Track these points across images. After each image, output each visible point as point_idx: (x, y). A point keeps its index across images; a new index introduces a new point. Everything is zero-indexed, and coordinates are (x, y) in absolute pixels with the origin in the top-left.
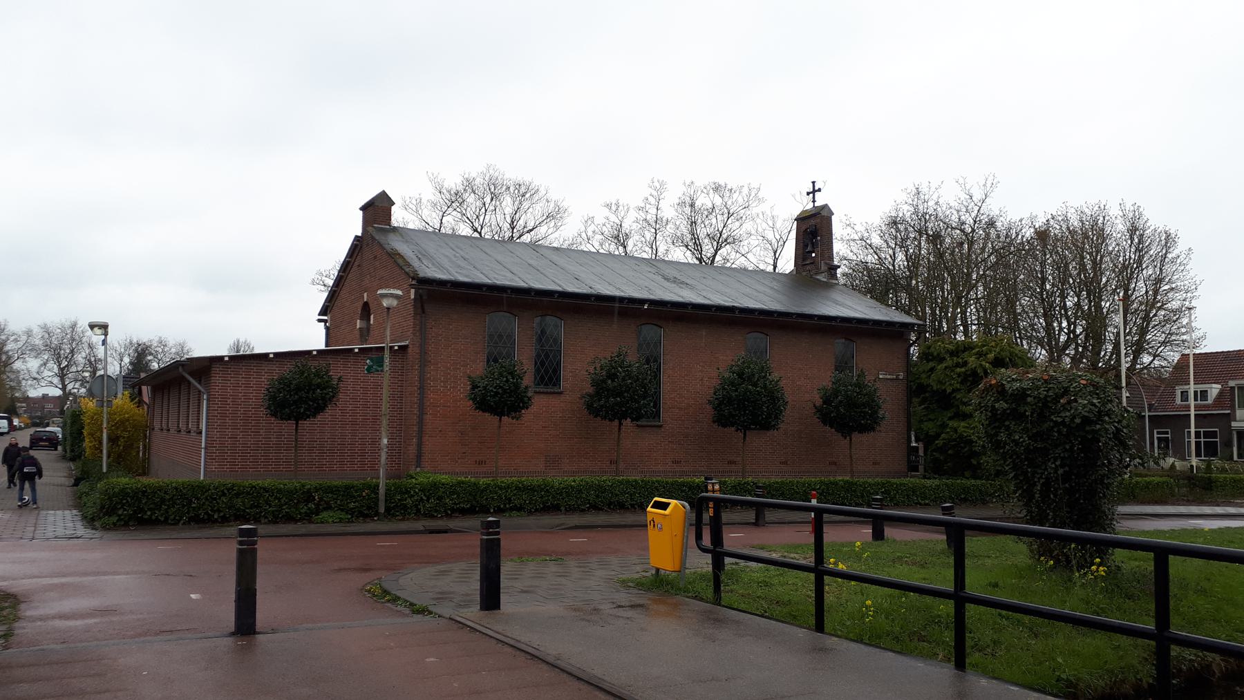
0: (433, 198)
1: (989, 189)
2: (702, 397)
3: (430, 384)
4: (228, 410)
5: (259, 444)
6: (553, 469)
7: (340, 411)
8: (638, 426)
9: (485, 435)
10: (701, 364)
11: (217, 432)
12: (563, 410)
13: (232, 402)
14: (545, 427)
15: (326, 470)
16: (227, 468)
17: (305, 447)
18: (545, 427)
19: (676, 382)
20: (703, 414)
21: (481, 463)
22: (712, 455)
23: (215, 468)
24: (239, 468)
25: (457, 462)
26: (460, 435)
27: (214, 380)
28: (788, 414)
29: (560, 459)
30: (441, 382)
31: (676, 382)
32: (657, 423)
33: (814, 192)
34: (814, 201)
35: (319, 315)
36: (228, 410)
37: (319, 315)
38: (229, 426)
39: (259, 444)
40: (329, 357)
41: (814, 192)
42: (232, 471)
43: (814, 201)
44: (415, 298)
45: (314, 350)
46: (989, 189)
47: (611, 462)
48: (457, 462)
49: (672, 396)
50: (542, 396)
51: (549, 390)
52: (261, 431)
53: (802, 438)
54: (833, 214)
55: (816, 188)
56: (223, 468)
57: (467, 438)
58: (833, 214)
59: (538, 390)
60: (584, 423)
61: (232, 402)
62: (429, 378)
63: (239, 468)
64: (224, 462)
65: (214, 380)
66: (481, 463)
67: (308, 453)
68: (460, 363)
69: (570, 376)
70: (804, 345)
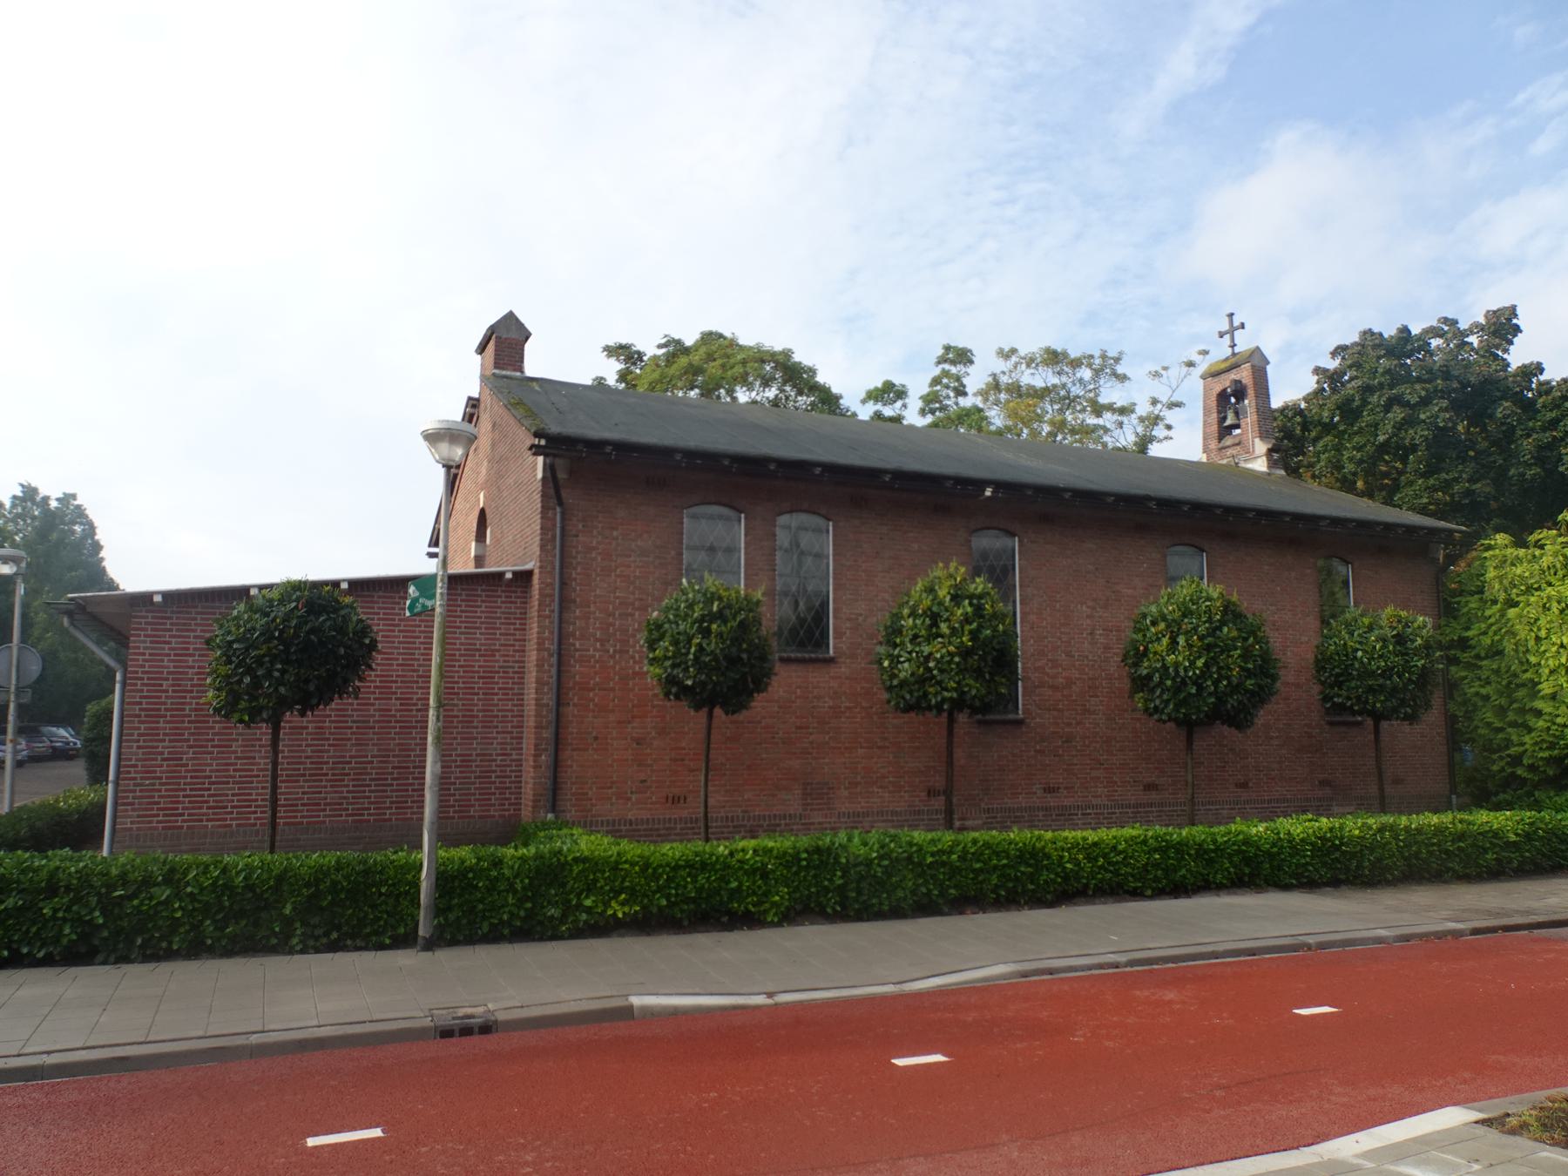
0: (966, 716)
1: (1503, 326)
2: (1093, 666)
3: (574, 645)
4: (165, 704)
5: (228, 770)
6: (819, 810)
7: (398, 702)
8: (979, 722)
9: (683, 745)
10: (1090, 603)
11: (139, 747)
12: (835, 693)
13: (173, 685)
14: (800, 728)
15: (231, 825)
16: (158, 822)
17: (327, 775)
18: (800, 728)
19: (1046, 637)
20: (1098, 697)
21: (675, 800)
22: (1115, 774)
23: (132, 823)
24: (184, 821)
25: (629, 799)
26: (635, 745)
27: (135, 642)
28: (1287, 676)
29: (829, 788)
30: (597, 640)
31: (1046, 637)
32: (1011, 716)
33: (1232, 331)
34: (1233, 346)
35: (430, 546)
36: (165, 704)
37: (430, 546)
38: (165, 734)
39: (228, 770)
40: (376, 594)
41: (1232, 331)
42: (170, 828)
43: (1233, 346)
44: (544, 478)
45: (344, 580)
46: (1503, 326)
47: (929, 792)
48: (629, 799)
49: (1038, 664)
50: (793, 667)
51: (806, 656)
52: (234, 744)
53: (1272, 738)
54: (1268, 363)
55: (1227, 337)
56: (150, 822)
57: (649, 751)
58: (1268, 363)
59: (785, 655)
60: (875, 718)
61: (173, 685)
62: (573, 634)
63: (184, 821)
64: (152, 809)
65: (135, 642)
66: (675, 800)
67: (331, 786)
68: (633, 604)
69: (847, 628)
70: (1266, 567)
